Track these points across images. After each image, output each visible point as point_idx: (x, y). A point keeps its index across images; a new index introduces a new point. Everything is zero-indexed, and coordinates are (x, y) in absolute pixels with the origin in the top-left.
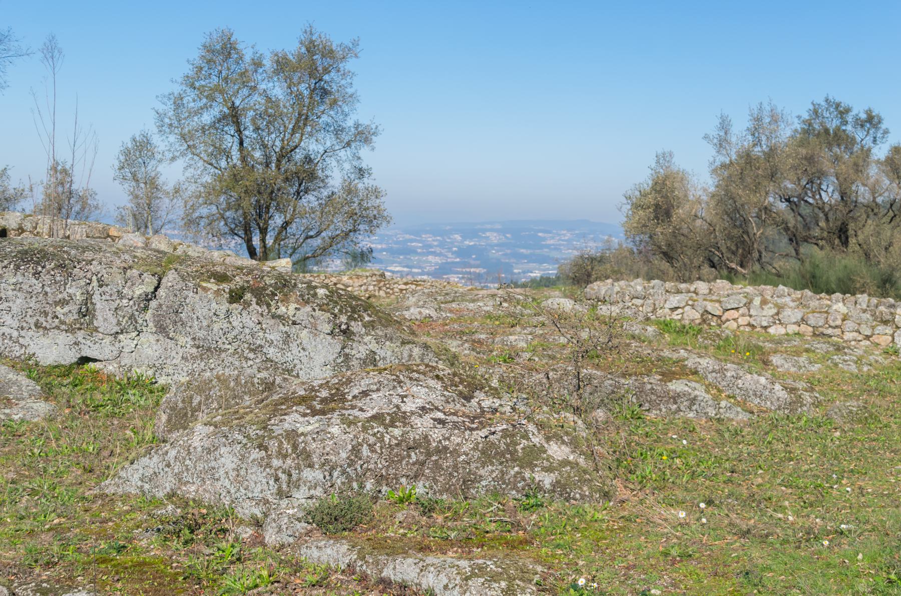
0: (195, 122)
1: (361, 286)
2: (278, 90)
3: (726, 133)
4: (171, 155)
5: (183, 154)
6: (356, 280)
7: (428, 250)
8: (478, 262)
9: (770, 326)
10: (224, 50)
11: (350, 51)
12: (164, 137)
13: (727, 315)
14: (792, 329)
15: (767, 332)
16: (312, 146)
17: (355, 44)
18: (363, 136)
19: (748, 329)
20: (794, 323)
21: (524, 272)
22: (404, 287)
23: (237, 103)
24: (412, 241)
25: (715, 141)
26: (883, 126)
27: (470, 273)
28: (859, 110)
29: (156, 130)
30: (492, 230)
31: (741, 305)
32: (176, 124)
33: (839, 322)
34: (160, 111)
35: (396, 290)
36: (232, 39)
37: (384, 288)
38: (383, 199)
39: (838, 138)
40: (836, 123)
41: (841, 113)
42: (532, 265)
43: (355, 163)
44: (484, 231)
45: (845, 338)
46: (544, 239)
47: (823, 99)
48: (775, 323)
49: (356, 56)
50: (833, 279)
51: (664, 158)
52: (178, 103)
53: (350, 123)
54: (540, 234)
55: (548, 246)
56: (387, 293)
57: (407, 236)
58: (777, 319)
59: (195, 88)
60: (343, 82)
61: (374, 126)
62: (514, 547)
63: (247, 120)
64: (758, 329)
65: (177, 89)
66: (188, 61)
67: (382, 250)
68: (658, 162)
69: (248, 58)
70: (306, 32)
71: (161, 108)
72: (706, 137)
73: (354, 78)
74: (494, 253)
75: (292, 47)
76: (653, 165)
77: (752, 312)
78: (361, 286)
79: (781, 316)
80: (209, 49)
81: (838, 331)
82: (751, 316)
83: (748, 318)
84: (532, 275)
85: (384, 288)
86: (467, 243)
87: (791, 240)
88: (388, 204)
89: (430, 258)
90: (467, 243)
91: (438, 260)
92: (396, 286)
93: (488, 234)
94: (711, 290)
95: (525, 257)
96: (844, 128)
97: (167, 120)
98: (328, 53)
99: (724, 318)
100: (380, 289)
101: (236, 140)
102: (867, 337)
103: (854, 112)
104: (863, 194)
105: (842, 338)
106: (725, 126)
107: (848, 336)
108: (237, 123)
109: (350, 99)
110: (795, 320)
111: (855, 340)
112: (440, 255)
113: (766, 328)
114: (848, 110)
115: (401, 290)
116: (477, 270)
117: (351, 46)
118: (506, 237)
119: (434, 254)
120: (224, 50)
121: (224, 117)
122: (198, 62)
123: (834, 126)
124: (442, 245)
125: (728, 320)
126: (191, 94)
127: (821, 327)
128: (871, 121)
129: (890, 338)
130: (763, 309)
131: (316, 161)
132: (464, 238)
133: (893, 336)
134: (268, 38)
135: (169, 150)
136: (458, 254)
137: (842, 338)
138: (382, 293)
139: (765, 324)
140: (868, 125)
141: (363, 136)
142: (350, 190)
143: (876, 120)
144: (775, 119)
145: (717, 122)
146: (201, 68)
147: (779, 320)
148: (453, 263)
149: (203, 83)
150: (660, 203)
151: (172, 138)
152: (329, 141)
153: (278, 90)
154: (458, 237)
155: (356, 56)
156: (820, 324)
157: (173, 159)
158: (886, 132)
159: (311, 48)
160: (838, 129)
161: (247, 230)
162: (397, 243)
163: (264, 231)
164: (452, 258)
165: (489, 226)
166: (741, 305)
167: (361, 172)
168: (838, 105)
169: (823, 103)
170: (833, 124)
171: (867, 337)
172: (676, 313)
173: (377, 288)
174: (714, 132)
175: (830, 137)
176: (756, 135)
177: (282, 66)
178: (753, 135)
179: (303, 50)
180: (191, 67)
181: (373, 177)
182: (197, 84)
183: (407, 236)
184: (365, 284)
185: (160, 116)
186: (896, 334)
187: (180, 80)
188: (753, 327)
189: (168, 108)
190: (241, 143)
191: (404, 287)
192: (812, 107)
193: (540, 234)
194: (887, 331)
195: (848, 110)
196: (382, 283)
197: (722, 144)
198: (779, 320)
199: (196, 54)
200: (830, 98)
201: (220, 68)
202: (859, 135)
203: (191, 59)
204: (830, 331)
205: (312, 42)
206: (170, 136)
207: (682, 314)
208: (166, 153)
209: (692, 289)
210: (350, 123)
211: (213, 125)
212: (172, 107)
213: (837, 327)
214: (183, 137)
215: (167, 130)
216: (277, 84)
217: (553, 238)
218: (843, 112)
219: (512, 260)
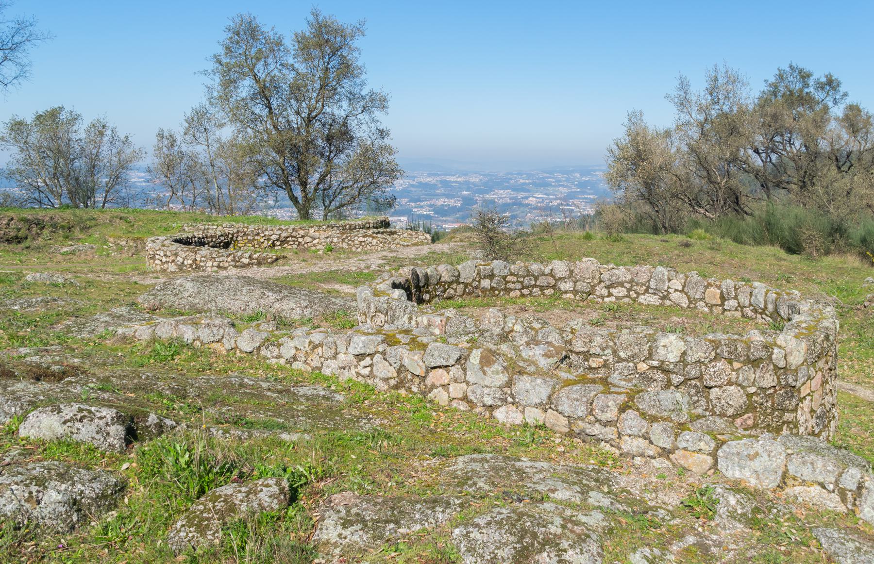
3: (685, 92)
7: (559, 184)
9: (498, 407)
10: (246, 32)
11: (359, 30)
13: (435, 377)
14: (534, 416)
15: (492, 417)
16: (339, 110)
17: (362, 24)
18: (379, 102)
19: (463, 406)
20: (537, 406)
24: (548, 178)
25: (676, 100)
26: (842, 89)
27: (586, 198)
28: (819, 74)
30: (599, 170)
31: (451, 362)
33: (612, 415)
35: (356, 242)
38: (395, 156)
39: (804, 100)
40: (799, 86)
41: (803, 77)
44: (595, 171)
45: (625, 448)
47: (788, 65)
48: (506, 400)
50: (786, 227)
51: (634, 118)
56: (349, 245)
57: (545, 175)
58: (507, 396)
64: (479, 409)
66: (218, 42)
67: (530, 184)
68: (630, 119)
72: (667, 96)
76: (626, 122)
77: (470, 377)
79: (515, 389)
81: (610, 432)
82: (468, 383)
83: (464, 385)
87: (762, 186)
88: (398, 159)
89: (561, 189)
91: (565, 190)
94: (571, 272)
96: (806, 90)
99: (428, 381)
102: (665, 453)
103: (815, 76)
104: (824, 146)
105: (619, 448)
106: (684, 86)
107: (630, 445)
110: (538, 401)
111: (642, 455)
112: (567, 187)
113: (491, 408)
114: (809, 75)
115: (361, 242)
119: (563, 186)
120: (246, 32)
123: (797, 88)
124: (567, 180)
125: (434, 386)
127: (580, 418)
128: (831, 84)
129: (710, 460)
130: (485, 373)
133: (714, 455)
136: (578, 186)
137: (619, 448)
139: (489, 401)
140: (828, 87)
141: (379, 102)
143: (835, 84)
144: (733, 80)
145: (677, 83)
147: (512, 396)
148: (575, 192)
150: (636, 156)
154: (578, 175)
156: (580, 414)
158: (845, 95)
160: (801, 91)
162: (538, 179)
164: (574, 189)
165: (597, 168)
166: (451, 362)
168: (800, 72)
169: (788, 69)
170: (797, 86)
171: (665, 453)
172: (363, 363)
174: (674, 93)
175: (795, 99)
176: (715, 94)
178: (711, 94)
181: (391, 136)
183: (545, 175)
186: (720, 453)
188: (472, 404)
191: (362, 239)
192: (777, 72)
194: (702, 445)
195: (809, 75)
197: (683, 103)
198: (512, 396)
199: (224, 36)
200: (794, 64)
202: (819, 95)
204: (596, 430)
207: (371, 365)
209: (547, 271)
213: (606, 424)
218: (804, 76)
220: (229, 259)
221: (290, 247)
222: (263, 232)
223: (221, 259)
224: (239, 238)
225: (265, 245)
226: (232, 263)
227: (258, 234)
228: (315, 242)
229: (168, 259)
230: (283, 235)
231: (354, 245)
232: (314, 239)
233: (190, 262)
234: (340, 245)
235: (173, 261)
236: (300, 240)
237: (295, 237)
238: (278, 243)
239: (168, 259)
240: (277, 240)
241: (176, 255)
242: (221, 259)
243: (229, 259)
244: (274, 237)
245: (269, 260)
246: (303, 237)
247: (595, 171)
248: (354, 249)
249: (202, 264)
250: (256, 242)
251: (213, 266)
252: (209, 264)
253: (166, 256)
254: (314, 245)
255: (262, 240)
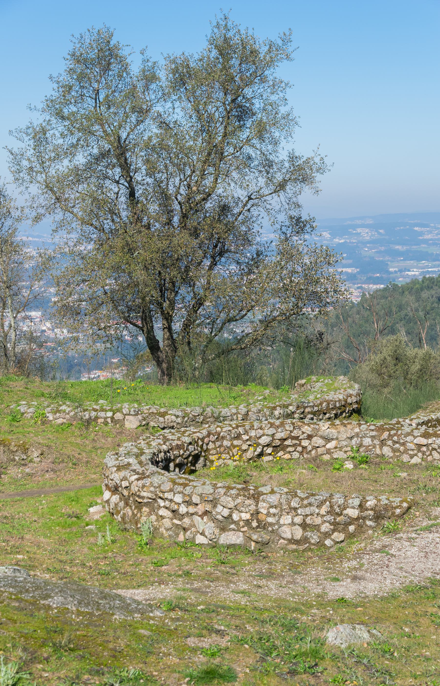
0: (64, 166)
1: (351, 438)
2: (178, 112)
4: (34, 214)
5: (50, 210)
6: (342, 429)
8: (350, 261)
10: (99, 59)
11: (278, 51)
12: (23, 188)
16: (232, 189)
17: (286, 39)
21: (401, 271)
22: (423, 441)
23: (124, 136)
29: (10, 178)
32: (38, 168)
34: (15, 150)
36: (112, 43)
37: (390, 443)
42: (409, 263)
43: (294, 213)
44: (355, 227)
46: (421, 234)
49: (288, 57)
52: (40, 136)
53: (282, 155)
54: (416, 229)
55: (426, 241)
59: (63, 118)
60: (274, 98)
61: (317, 160)
62: (64, 119)
63: (137, 160)
65: (39, 119)
66: (51, 78)
69: (135, 68)
70: (218, 26)
71: (17, 146)
73: (288, 89)
74: (367, 252)
75: (196, 47)
78: (351, 438)
80: (78, 58)
84: (410, 273)
85: (390, 443)
86: (336, 240)
90: (336, 240)
92: (409, 438)
93: (359, 230)
95: (399, 254)
97: (25, 163)
98: (250, 55)
100: (383, 443)
101: (124, 191)
108: (125, 167)
109: (283, 121)
115: (419, 446)
116: (349, 270)
117: (280, 42)
118: (379, 233)
120: (99, 59)
121: (103, 155)
122: (65, 78)
126: (58, 128)
131: (236, 211)
132: (334, 235)
134: (163, 39)
135: (32, 207)
138: (386, 451)
141: (301, 173)
142: (288, 254)
146: (70, 88)
149: (73, 109)
151: (34, 189)
152: (257, 181)
153: (178, 112)
155: (288, 57)
157: (37, 219)
159: (225, 48)
161: (147, 319)
163: (168, 318)
165: (359, 222)
167: (299, 225)
173: (377, 442)
177: (183, 76)
179: (214, 53)
180: (55, 86)
182: (66, 112)
184: (357, 435)
185: (16, 157)
187: (40, 106)
189: (26, 145)
190: (132, 194)
191: (423, 441)
193: (416, 229)
196: (386, 435)
199: (60, 67)
201: (96, 85)
203: (55, 75)
205: (226, 40)
206: (31, 185)
208: (27, 211)
210: (282, 155)
211: (89, 166)
212: (32, 142)
214: (49, 187)
215: (27, 178)
216: (177, 104)
217: (431, 232)
219: (387, 258)
220: (324, 510)
221: (287, 456)
222: (246, 432)
223: (308, 511)
224: (211, 446)
225: (249, 454)
226: (329, 518)
227: (239, 436)
228: (329, 446)
229: (191, 510)
230: (279, 435)
231: (406, 451)
232: (328, 440)
233: (246, 516)
234: (378, 451)
235: (206, 513)
236: (305, 443)
237: (297, 438)
238: (269, 450)
239: (191, 510)
240: (268, 445)
241: (214, 502)
242: (308, 511)
243: (324, 510)
244: (264, 440)
245: (398, 511)
246: (310, 437)
247: (355, 227)
248: (405, 458)
249: (270, 520)
250: (235, 451)
251: (293, 524)
252: (286, 519)
253: (188, 503)
254: (329, 452)
255: (244, 447)
